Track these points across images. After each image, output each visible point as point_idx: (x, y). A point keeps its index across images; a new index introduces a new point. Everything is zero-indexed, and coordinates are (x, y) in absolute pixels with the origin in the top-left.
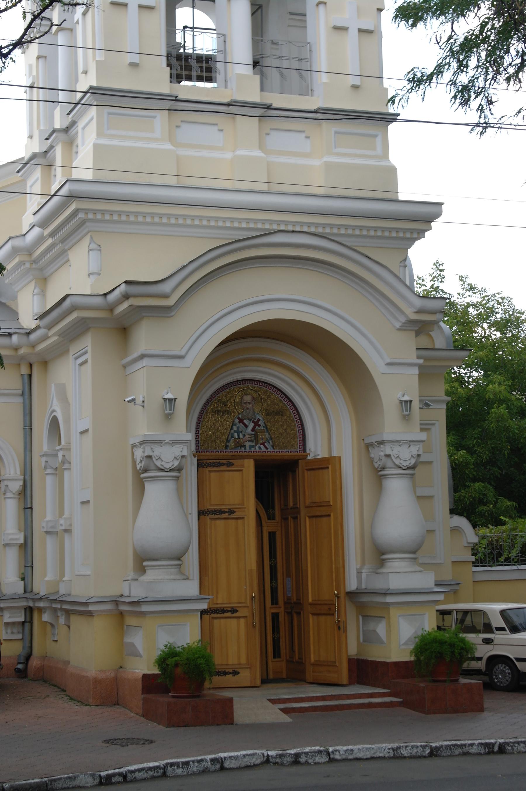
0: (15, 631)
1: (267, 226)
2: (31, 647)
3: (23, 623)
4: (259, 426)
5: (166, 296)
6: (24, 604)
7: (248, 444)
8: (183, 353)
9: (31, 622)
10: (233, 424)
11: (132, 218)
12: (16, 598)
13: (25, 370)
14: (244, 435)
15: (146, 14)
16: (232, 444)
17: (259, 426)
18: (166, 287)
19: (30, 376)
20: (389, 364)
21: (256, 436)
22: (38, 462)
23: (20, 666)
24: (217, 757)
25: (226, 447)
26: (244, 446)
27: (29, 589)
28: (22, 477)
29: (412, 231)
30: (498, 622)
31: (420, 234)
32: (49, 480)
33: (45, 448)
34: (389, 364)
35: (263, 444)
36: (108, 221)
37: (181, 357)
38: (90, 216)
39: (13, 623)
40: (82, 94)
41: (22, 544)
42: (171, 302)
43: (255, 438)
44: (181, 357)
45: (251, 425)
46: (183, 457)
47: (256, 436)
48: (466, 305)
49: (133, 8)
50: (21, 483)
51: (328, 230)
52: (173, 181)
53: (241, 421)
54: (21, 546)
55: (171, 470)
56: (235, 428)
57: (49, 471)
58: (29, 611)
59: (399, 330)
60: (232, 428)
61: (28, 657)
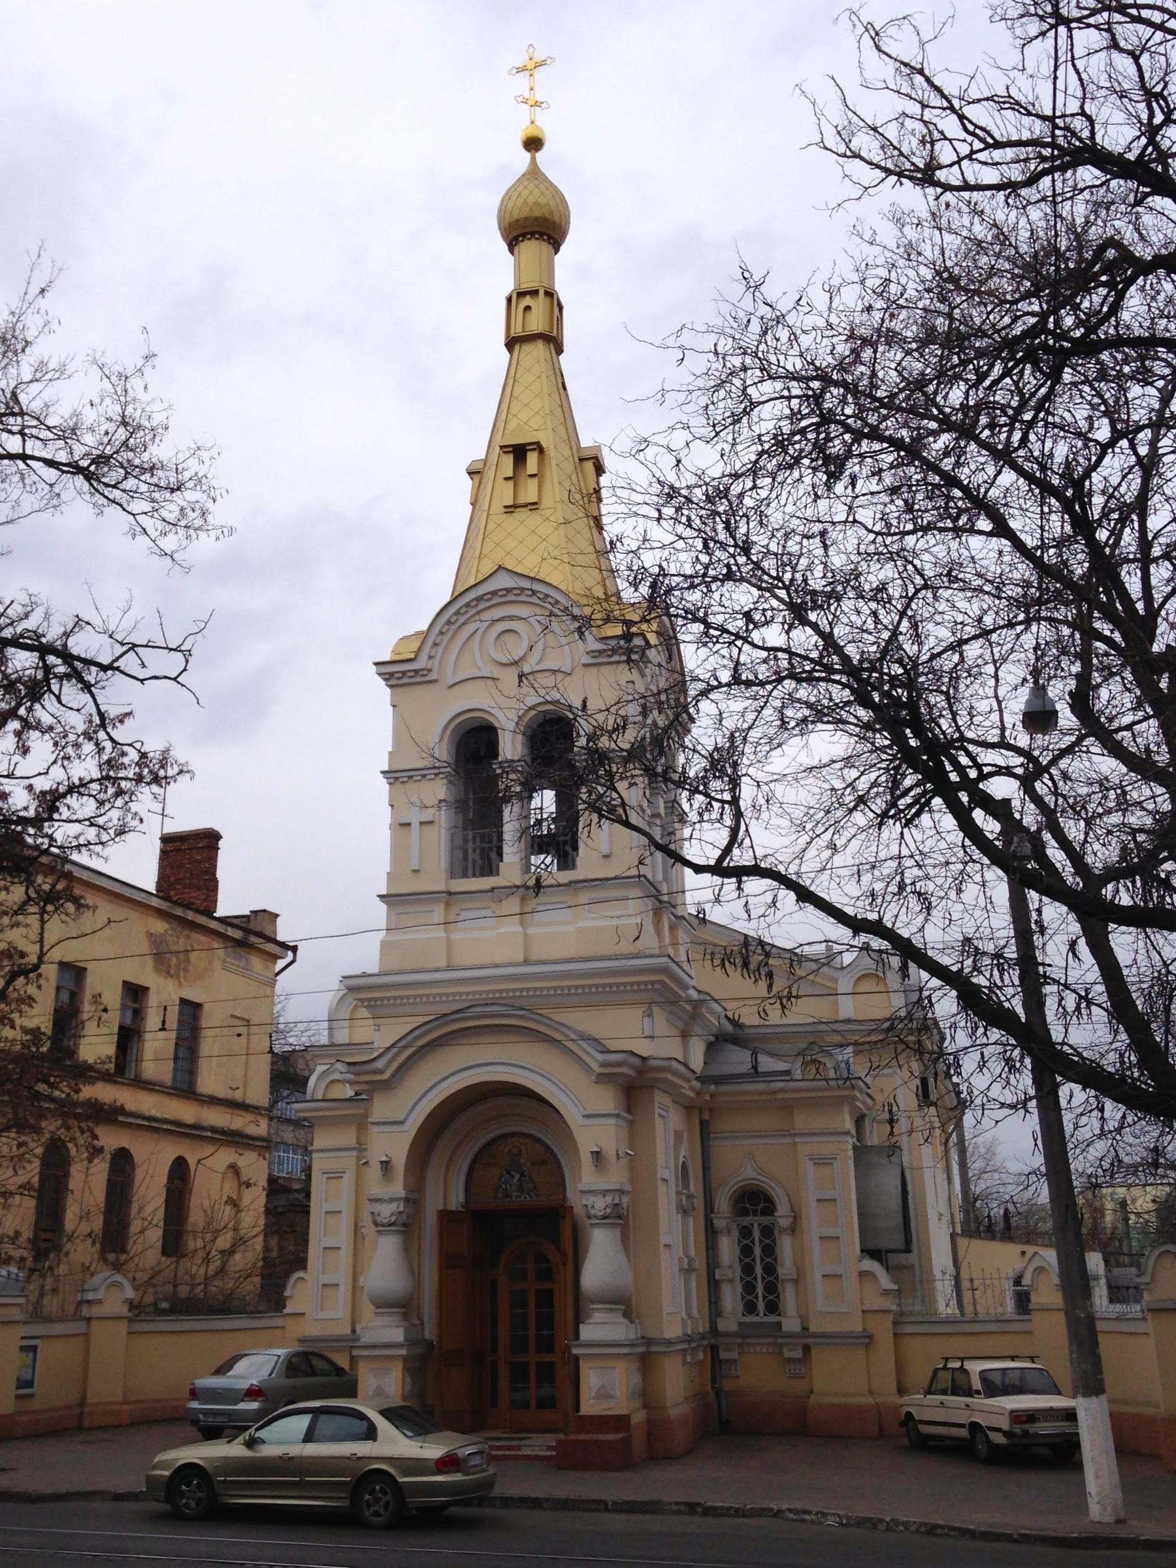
5: (381, 1072)
8: (401, 1119)
10: (502, 1175)
15: (427, 828)
16: (500, 1195)
18: (379, 1064)
20: (585, 1116)
26: (511, 1196)
30: (977, 1384)
34: (585, 1116)
37: (401, 1123)
42: (386, 1076)
43: (521, 1189)
44: (401, 1123)
45: (517, 1177)
49: (415, 826)
53: (508, 1173)
54: (718, 1267)
55: (389, 1225)
60: (500, 1179)
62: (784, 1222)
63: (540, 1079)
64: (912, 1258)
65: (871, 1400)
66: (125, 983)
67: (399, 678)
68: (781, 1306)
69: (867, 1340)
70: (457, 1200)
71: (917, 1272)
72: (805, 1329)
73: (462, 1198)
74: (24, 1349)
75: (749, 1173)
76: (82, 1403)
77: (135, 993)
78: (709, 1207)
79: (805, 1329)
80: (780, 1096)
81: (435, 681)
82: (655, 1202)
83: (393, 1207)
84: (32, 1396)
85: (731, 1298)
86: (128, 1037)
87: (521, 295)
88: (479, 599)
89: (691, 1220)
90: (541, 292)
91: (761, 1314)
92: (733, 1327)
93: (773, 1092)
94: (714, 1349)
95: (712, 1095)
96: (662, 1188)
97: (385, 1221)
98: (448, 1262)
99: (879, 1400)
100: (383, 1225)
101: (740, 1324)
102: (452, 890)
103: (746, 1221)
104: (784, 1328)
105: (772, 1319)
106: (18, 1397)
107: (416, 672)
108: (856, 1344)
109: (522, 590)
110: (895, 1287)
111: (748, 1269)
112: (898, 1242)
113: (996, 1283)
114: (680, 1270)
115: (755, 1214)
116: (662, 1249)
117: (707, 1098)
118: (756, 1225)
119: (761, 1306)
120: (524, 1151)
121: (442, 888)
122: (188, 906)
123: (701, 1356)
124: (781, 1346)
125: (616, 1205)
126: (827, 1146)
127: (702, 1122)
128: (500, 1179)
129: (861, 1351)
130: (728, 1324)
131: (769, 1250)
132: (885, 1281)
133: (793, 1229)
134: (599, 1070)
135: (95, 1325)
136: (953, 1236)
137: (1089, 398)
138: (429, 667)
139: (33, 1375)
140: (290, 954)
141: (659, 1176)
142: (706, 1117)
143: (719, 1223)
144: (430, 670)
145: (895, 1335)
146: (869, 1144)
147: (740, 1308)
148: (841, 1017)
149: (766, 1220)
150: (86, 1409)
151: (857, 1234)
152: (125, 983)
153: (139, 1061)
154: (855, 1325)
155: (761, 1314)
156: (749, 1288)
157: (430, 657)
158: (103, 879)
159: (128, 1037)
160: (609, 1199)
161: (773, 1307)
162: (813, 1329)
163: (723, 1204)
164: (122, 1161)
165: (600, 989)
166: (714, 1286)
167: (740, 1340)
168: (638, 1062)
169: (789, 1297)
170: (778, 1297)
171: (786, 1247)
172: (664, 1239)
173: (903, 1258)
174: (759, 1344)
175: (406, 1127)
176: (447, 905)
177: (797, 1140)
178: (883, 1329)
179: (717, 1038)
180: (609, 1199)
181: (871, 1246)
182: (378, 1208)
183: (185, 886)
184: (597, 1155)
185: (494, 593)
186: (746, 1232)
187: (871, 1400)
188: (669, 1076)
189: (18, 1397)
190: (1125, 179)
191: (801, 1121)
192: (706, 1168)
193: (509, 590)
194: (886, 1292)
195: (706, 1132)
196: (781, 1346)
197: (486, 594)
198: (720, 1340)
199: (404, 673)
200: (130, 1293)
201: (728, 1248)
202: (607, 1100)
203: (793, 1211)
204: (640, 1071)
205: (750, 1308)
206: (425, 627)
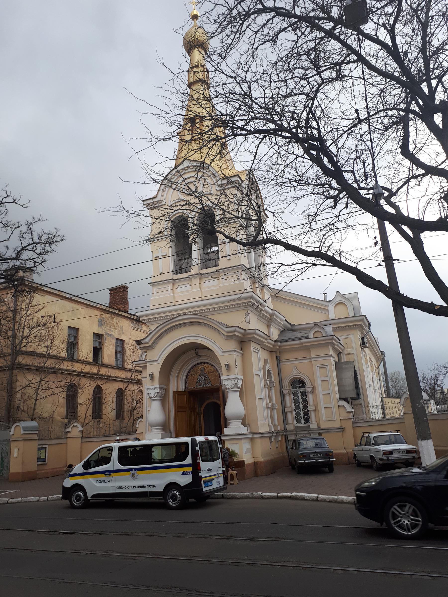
1: (173, 316)
5: (147, 343)
7: (203, 384)
8: (156, 359)
16: (198, 385)
18: (147, 340)
20: (222, 352)
34: (222, 352)
36: (216, 311)
37: (157, 361)
41: (226, 427)
44: (157, 361)
47: (205, 381)
51: (196, 312)
52: (173, 304)
53: (200, 377)
54: (286, 407)
55: (155, 397)
62: (309, 390)
63: (214, 346)
64: (361, 401)
65: (345, 451)
66: (94, 333)
68: (310, 420)
69: (343, 430)
70: (182, 387)
71: (363, 406)
72: (319, 427)
73: (184, 387)
74: (39, 449)
75: (295, 373)
77: (98, 337)
78: (281, 386)
79: (319, 427)
80: (304, 345)
82: (253, 383)
83: (155, 391)
84: (46, 464)
85: (291, 418)
86: (97, 351)
87: (192, 68)
89: (273, 391)
90: (200, 66)
91: (303, 423)
92: (292, 428)
93: (302, 344)
94: (286, 436)
95: (280, 347)
96: (256, 378)
97: (153, 396)
98: (178, 409)
99: (348, 451)
100: (152, 398)
101: (295, 427)
102: (175, 278)
103: (295, 390)
104: (311, 427)
105: (307, 424)
106: (38, 465)
107: (157, 202)
108: (337, 431)
110: (353, 410)
111: (297, 407)
112: (354, 395)
113: (391, 405)
114: (267, 408)
116: (257, 400)
117: (277, 347)
119: (303, 420)
120: (205, 368)
121: (171, 278)
122: (120, 310)
123: (280, 439)
124: (310, 434)
125: (236, 384)
126: (322, 361)
127: (277, 357)
129: (340, 434)
130: (290, 427)
131: (305, 401)
132: (348, 407)
133: (313, 392)
134: (226, 334)
136: (382, 398)
138: (162, 199)
139: (46, 456)
141: (254, 373)
142: (278, 355)
143: (285, 392)
145: (353, 427)
146: (343, 361)
147: (295, 421)
148: (330, 318)
149: (303, 390)
151: (338, 393)
152: (94, 333)
153: (103, 358)
154: (337, 424)
155: (303, 423)
156: (298, 414)
157: (162, 196)
158: (82, 299)
159: (97, 351)
160: (233, 382)
161: (307, 420)
162: (322, 426)
163: (286, 384)
164: (98, 391)
166: (285, 414)
167: (295, 433)
168: (243, 331)
169: (313, 416)
170: (309, 417)
171: (310, 398)
172: (258, 396)
173: (358, 401)
175: (159, 362)
176: (173, 284)
177: (312, 360)
178: (348, 425)
179: (284, 329)
180: (233, 382)
181: (344, 397)
182: (150, 391)
183: (118, 304)
184: (227, 366)
186: (295, 395)
187: (345, 451)
188: (255, 336)
189: (38, 465)
191: (314, 353)
192: (279, 373)
194: (349, 412)
195: (278, 360)
196: (310, 434)
198: (288, 433)
200: (80, 429)
201: (289, 400)
202: (233, 345)
203: (312, 385)
204: (244, 335)
205: (298, 421)
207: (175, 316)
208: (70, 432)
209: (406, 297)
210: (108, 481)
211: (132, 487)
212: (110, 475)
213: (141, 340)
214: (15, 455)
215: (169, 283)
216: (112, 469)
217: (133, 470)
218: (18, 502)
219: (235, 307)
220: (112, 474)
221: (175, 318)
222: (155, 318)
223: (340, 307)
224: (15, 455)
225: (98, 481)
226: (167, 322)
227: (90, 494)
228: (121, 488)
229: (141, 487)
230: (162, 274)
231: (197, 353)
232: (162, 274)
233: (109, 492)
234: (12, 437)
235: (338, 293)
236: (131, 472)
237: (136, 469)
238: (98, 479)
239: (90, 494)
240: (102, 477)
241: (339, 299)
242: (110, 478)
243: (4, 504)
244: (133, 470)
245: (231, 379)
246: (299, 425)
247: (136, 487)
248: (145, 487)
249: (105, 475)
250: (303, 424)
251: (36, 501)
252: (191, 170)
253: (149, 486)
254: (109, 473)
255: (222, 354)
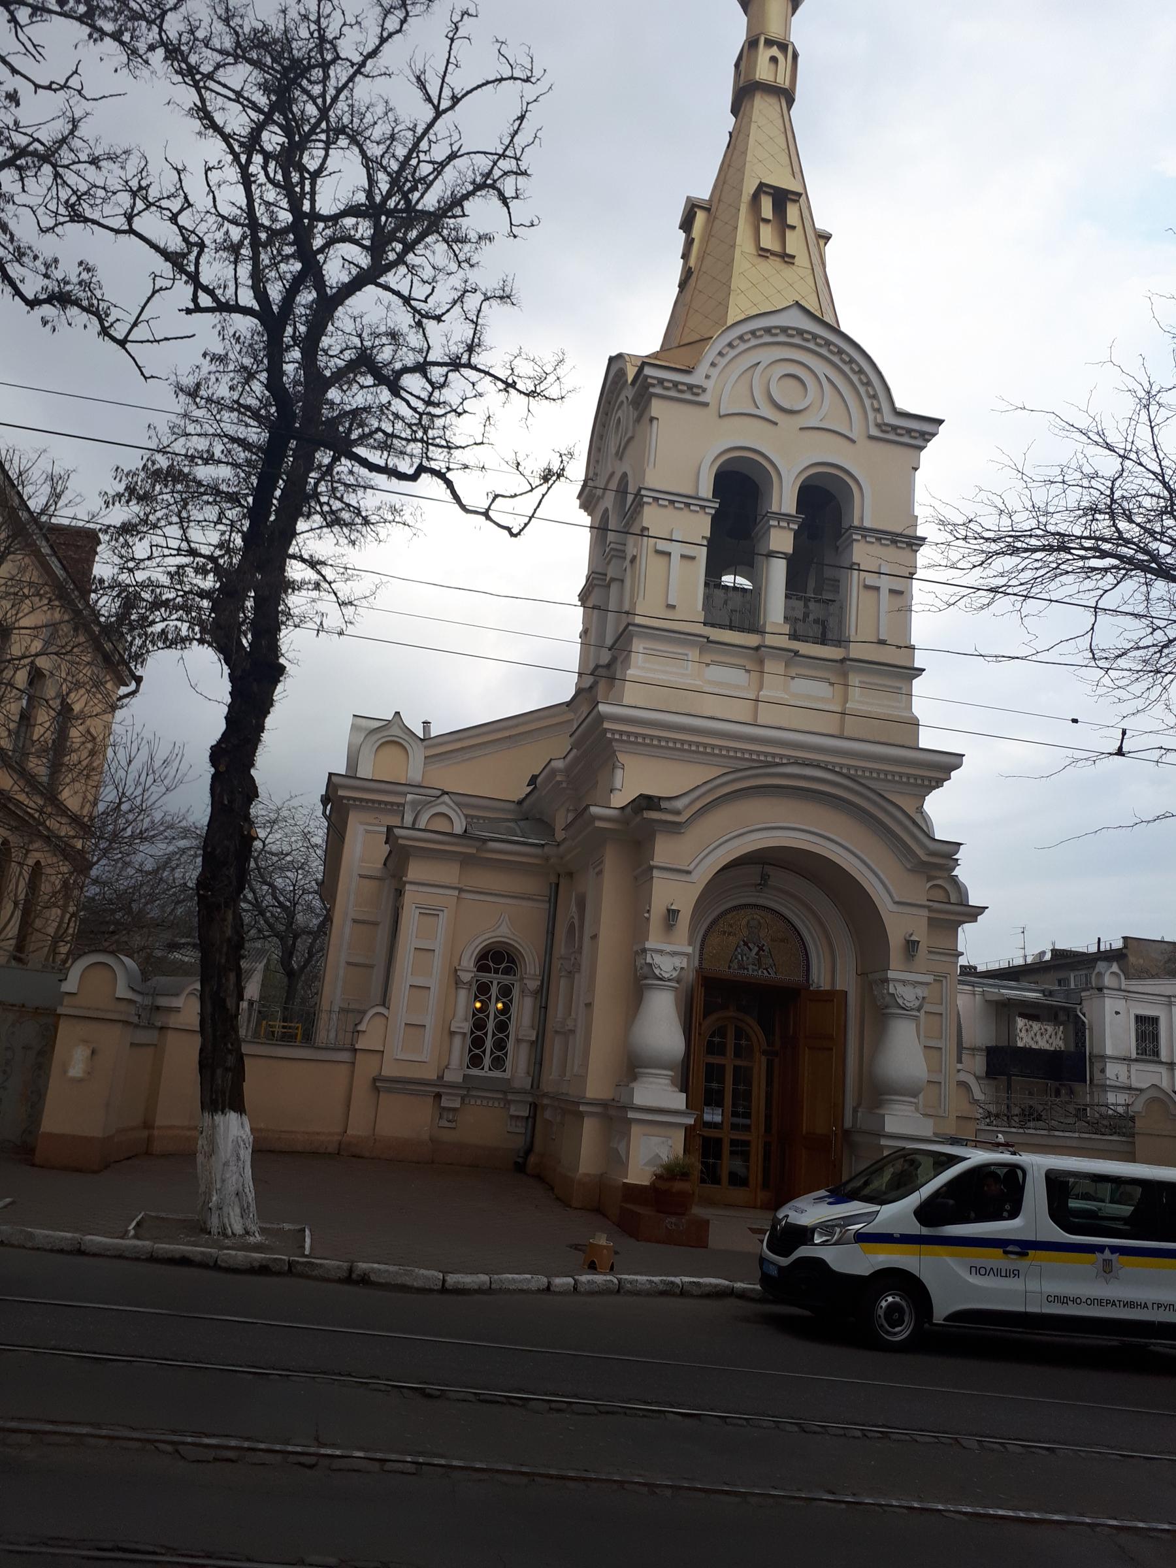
0: (519, 1124)
2: (532, 1143)
3: (527, 1118)
4: (763, 951)
6: (530, 1099)
7: (750, 967)
9: (534, 1118)
11: (655, 742)
12: (522, 1092)
13: (553, 879)
14: (748, 958)
16: (735, 965)
17: (763, 951)
19: (557, 885)
21: (759, 960)
22: (557, 964)
23: (520, 1160)
24: (1034, 1163)
25: (729, 967)
26: (747, 969)
27: (535, 1086)
28: (540, 978)
29: (930, 779)
31: (939, 783)
32: (563, 982)
33: (563, 951)
35: (766, 969)
37: (689, 872)
38: (617, 736)
39: (518, 1117)
40: (200, 293)
43: (759, 962)
44: (689, 872)
45: (756, 950)
46: (682, 968)
47: (759, 960)
48: (170, 62)
50: (539, 983)
51: (852, 772)
53: (746, 944)
54: (532, 1043)
56: (739, 950)
57: (563, 974)
58: (534, 1106)
59: (909, 870)
60: (736, 950)
61: (529, 1151)
67: (852, 369)
76: (148, 1125)
81: (706, 405)
88: (768, 330)
91: (486, 1068)
103: (485, 977)
107: (691, 387)
109: (815, 337)
115: (496, 971)
118: (495, 983)
119: (487, 1061)
128: (736, 950)
135: (171, 1036)
137: (399, 406)
140: (134, 684)
144: (704, 390)
149: (507, 979)
150: (156, 1132)
155: (486, 1068)
165: (678, 746)
174: (479, 1097)
175: (694, 877)
185: (784, 330)
190: (262, 324)
193: (801, 332)
197: (776, 327)
199: (676, 384)
205: (476, 1061)
206: (843, 328)
207: (785, 761)
208: (177, 1010)
209: (261, 728)
210: (1016, 1274)
211: (1100, 1302)
212: (1023, 1254)
213: (660, 798)
214: (77, 1070)
215: (693, 644)
216: (1030, 1237)
217: (1107, 1251)
218: (479, 1291)
219: (908, 784)
220: (1031, 1253)
221: (778, 765)
222: (652, 737)
223: (392, 752)
224: (77, 1070)
225: (977, 1270)
226: (757, 767)
227: (942, 1309)
228: (1063, 1300)
229: (1131, 1304)
230: (882, 642)
231: (764, 877)
232: (882, 642)
233: (1021, 1309)
234: (67, 1000)
235: (397, 716)
236: (1098, 1256)
237: (1114, 1249)
238: (979, 1262)
239: (942, 1309)
240: (995, 1258)
241: (395, 731)
242: (1021, 1264)
243: (431, 1291)
244: (1107, 1251)
245: (916, 984)
246: (475, 1072)
247: (1114, 1304)
248: (1146, 1306)
249: (1006, 1252)
250: (485, 1071)
251: (539, 1291)
252: (840, 364)
253: (1159, 1306)
254: (1024, 1247)
255: (892, 907)
